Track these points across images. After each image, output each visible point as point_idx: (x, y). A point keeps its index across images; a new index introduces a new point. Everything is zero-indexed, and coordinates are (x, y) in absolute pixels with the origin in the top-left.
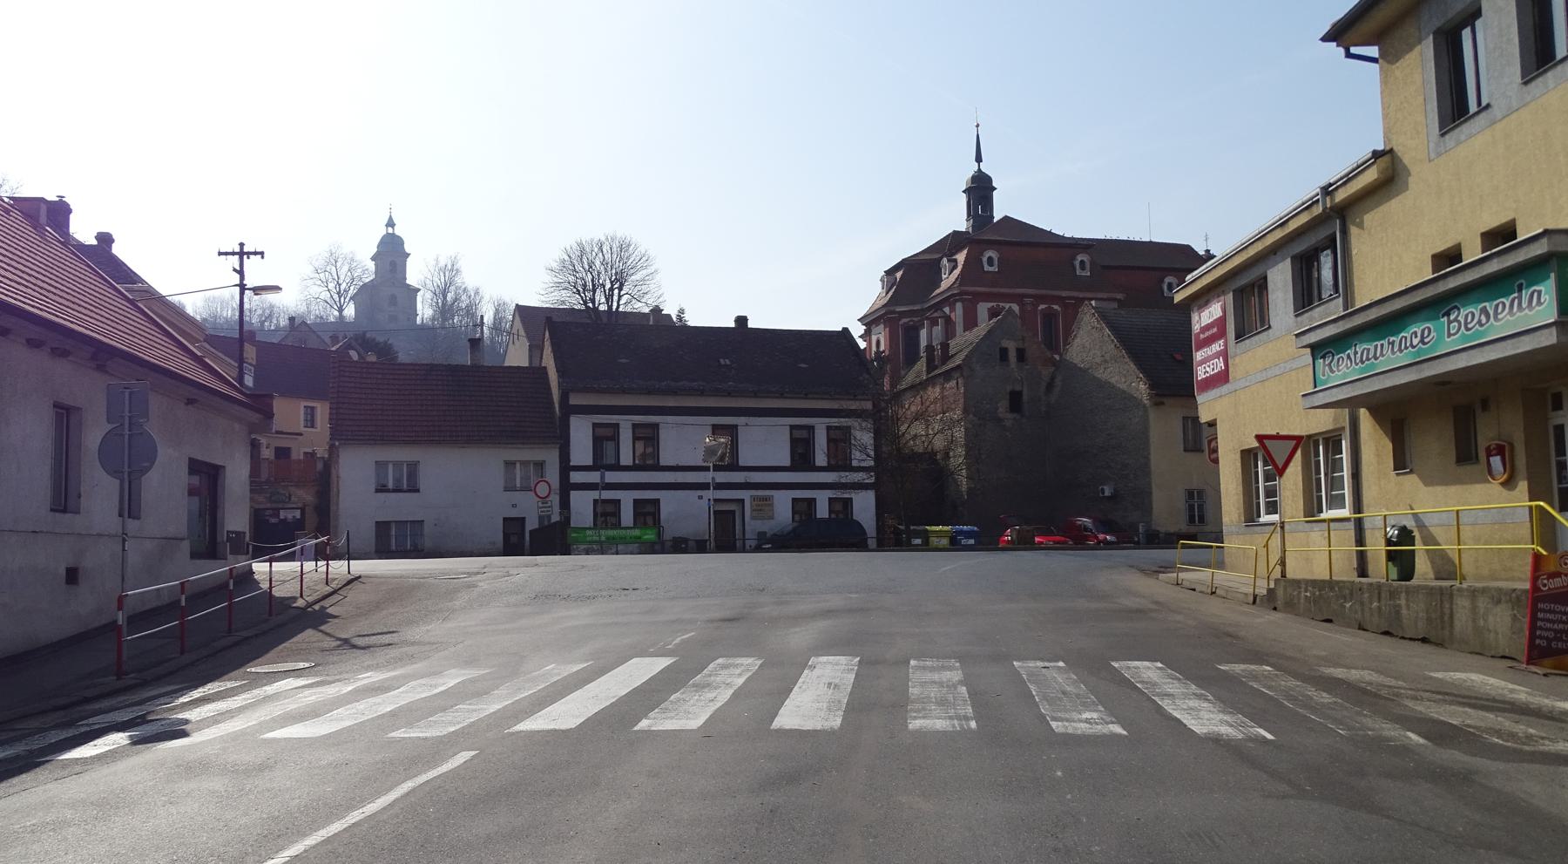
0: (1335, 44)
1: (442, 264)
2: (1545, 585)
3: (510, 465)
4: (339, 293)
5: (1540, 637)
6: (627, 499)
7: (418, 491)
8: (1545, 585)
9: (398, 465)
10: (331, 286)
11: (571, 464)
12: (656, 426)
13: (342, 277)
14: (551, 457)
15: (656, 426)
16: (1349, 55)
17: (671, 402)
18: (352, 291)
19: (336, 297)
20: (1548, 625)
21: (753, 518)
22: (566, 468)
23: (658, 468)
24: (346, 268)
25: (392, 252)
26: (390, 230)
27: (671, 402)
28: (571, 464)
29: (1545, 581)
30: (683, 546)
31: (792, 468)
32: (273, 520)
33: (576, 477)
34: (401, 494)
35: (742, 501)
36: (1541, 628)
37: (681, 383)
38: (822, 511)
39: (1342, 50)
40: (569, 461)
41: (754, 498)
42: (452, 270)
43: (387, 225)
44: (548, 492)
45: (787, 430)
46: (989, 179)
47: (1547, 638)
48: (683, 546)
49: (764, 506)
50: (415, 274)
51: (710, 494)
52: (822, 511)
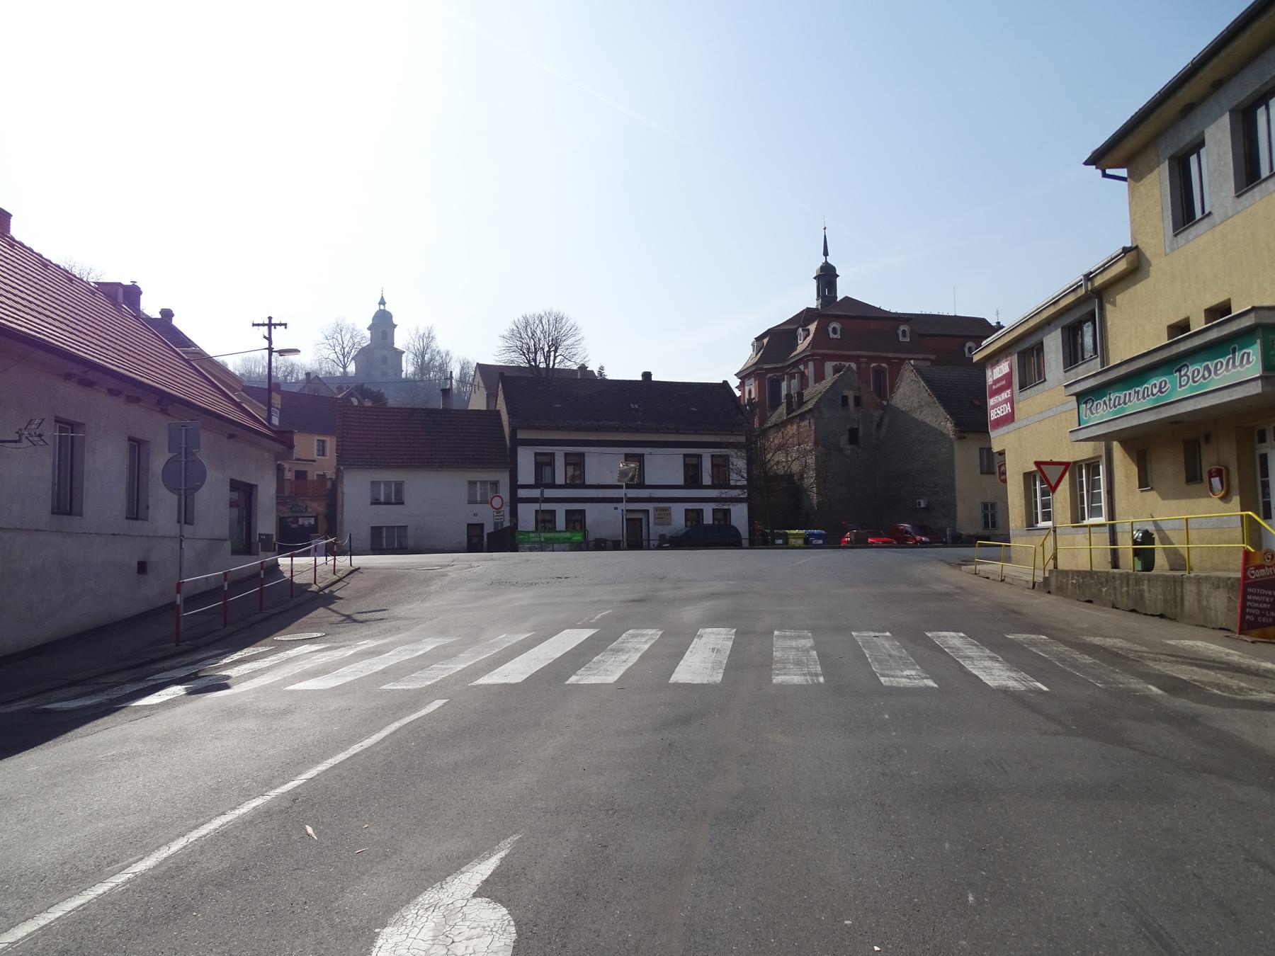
0: (1094, 167)
1: (421, 333)
2: (1253, 575)
3: (472, 484)
4: (343, 355)
5: (1249, 614)
6: (561, 510)
7: (403, 503)
8: (1253, 575)
9: (387, 484)
10: (338, 349)
11: (519, 483)
12: (582, 455)
13: (346, 343)
14: (503, 478)
15: (582, 455)
16: (1105, 175)
17: (594, 437)
18: (353, 353)
19: (341, 357)
20: (1256, 605)
21: (656, 524)
22: (514, 486)
23: (641, 485)
24: (348, 336)
25: (383, 324)
26: (382, 307)
27: (594, 437)
28: (519, 483)
29: (1253, 572)
30: (603, 545)
31: (685, 487)
32: (294, 526)
33: (522, 493)
34: (390, 507)
35: (647, 512)
36: (1250, 607)
37: (601, 423)
38: (708, 519)
39: (1099, 172)
40: (517, 481)
41: (656, 509)
42: (428, 337)
43: (380, 304)
44: (500, 500)
45: (681, 458)
46: (833, 269)
47: (1254, 615)
48: (603, 545)
49: (664, 516)
50: (401, 340)
51: (623, 506)
52: (708, 519)
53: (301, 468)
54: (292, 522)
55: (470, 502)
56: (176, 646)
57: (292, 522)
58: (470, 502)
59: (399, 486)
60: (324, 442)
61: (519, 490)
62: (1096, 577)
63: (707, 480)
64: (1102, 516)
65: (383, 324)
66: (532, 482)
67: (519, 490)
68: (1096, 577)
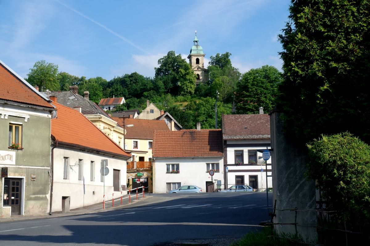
9: (173, 165)
11: (228, 164)
22: (226, 165)
25: (290, 17)
28: (228, 164)
53: (142, 155)
54: (137, 180)
55: (64, 179)
56: (275, 215)
57: (137, 180)
58: (64, 179)
59: (178, 166)
60: (137, 142)
61: (271, 169)
62: (306, 16)
63: (246, 161)
64: (12, 126)
65: (290, 17)
66: (234, 163)
67: (271, 169)
68: (306, 16)
